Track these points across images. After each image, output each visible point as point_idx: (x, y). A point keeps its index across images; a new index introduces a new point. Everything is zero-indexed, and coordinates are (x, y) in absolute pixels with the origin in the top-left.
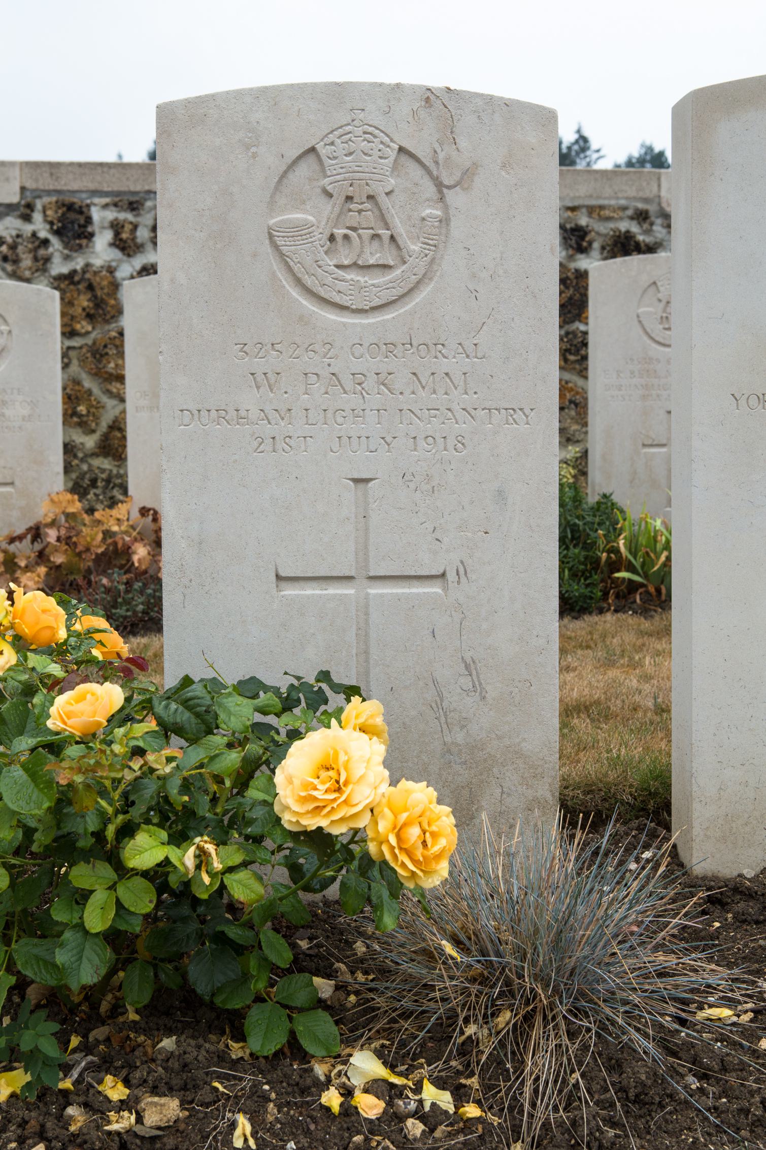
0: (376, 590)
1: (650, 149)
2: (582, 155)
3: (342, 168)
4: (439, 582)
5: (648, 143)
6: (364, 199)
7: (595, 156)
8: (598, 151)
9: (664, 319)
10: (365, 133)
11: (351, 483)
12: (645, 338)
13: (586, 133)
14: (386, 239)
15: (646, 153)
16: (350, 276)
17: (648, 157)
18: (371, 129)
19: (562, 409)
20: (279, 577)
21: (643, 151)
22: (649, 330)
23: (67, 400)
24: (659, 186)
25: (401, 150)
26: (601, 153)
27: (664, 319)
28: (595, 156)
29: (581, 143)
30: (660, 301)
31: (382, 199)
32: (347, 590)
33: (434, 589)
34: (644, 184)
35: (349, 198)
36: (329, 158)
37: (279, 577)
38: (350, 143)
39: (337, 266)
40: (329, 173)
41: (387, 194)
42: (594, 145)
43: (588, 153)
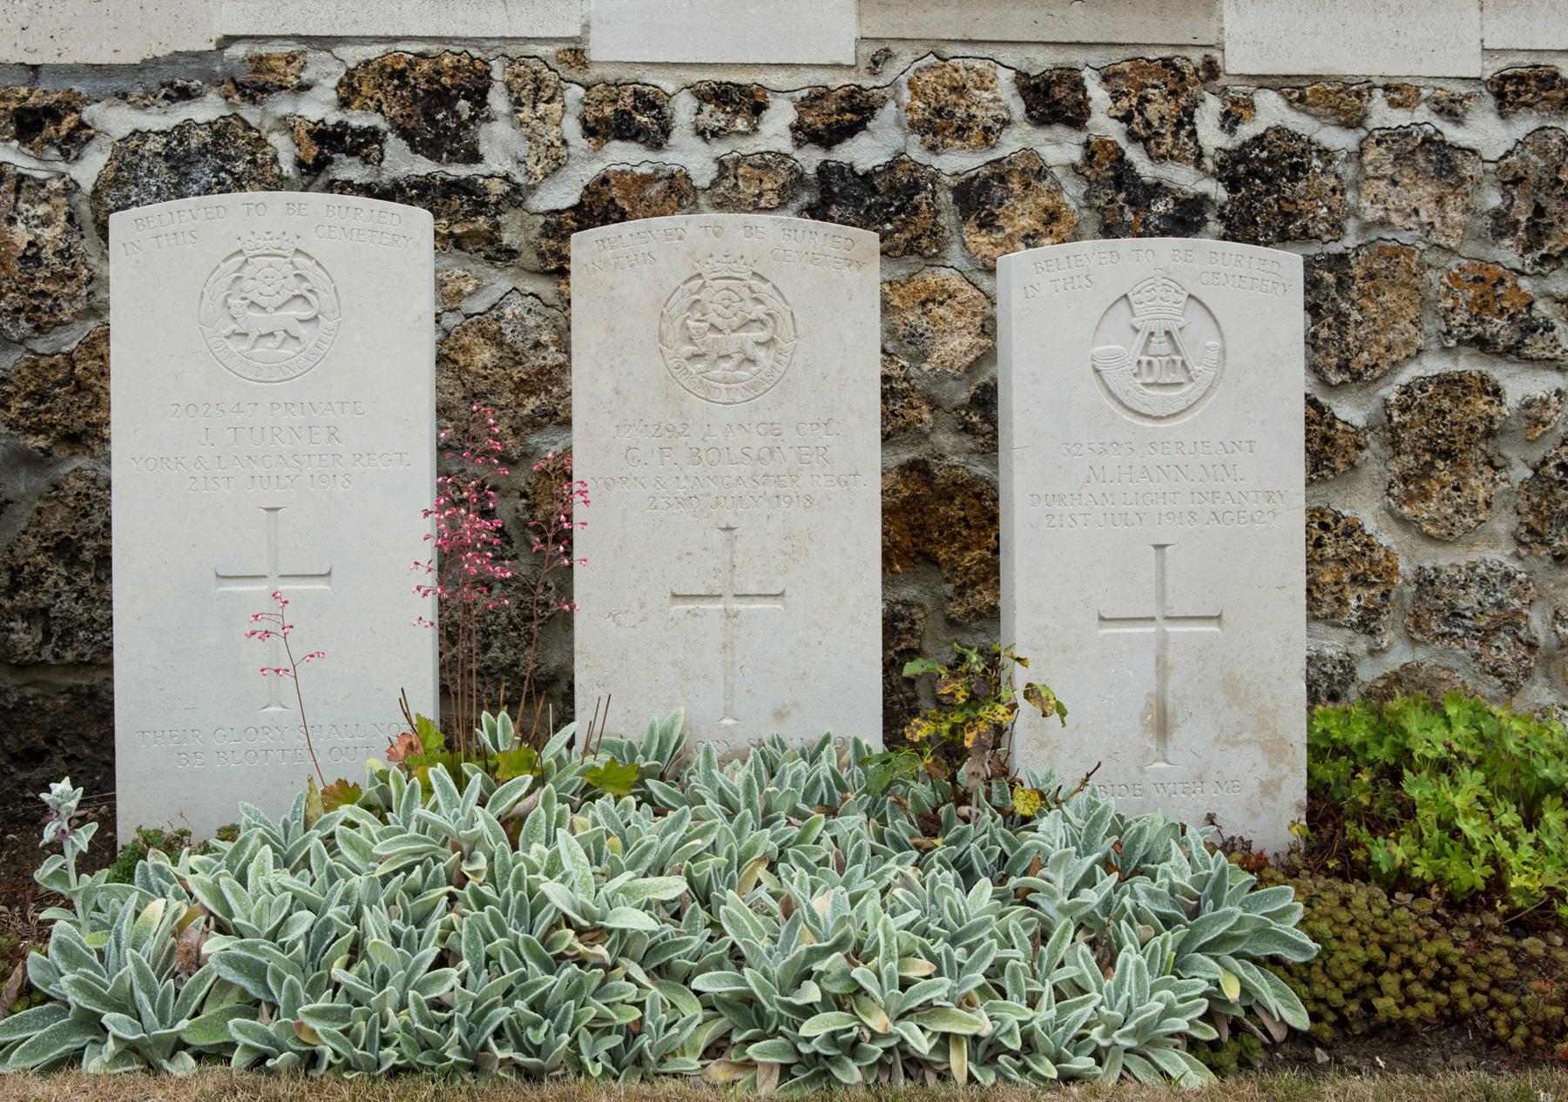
0: (1172, 629)
16: (1147, 391)
20: (1102, 619)
25: (1190, 296)
30: (1137, 331)
32: (1150, 629)
39: (1146, 385)
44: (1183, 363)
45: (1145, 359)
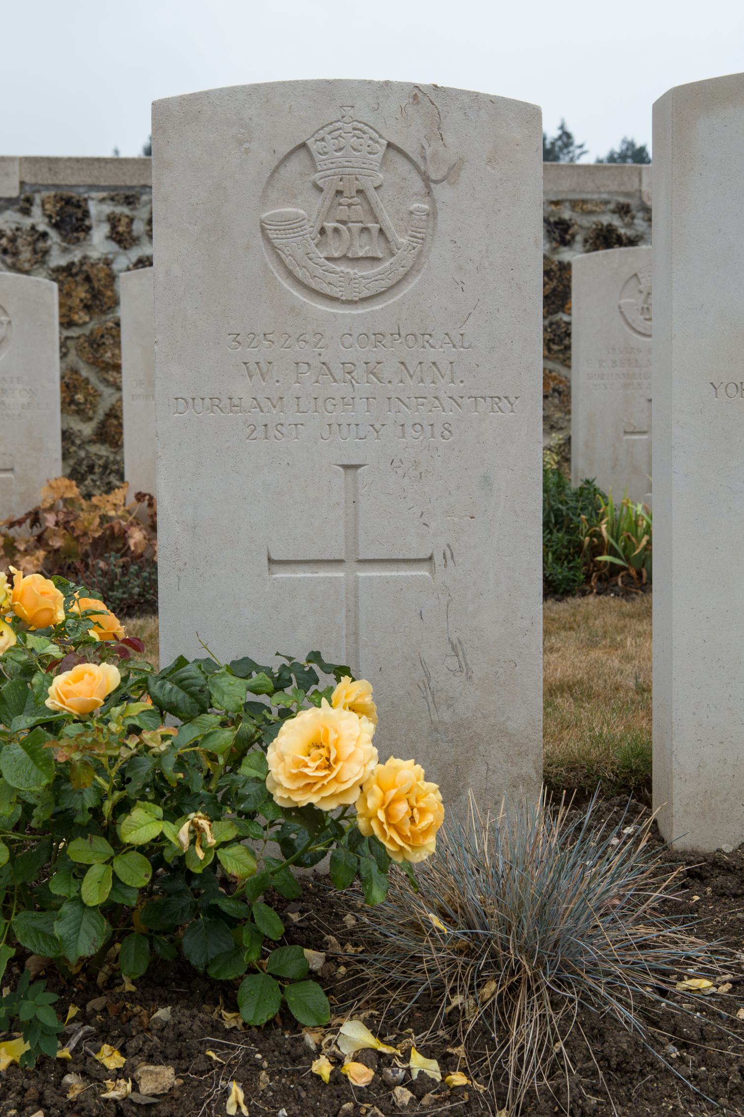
0: (365, 573)
1: (631, 145)
2: (565, 151)
3: (332, 163)
4: (426, 565)
5: (629, 139)
6: (354, 194)
7: (578, 151)
8: (581, 147)
9: (645, 310)
10: (354, 129)
11: (341, 469)
12: (627, 328)
13: (570, 129)
14: (375, 232)
15: (627, 149)
16: (341, 268)
17: (630, 153)
18: (360, 126)
19: (545, 397)
20: (271, 561)
21: (624, 147)
22: (630, 321)
23: (65, 389)
24: (640, 181)
25: (390, 145)
26: (585, 148)
27: (645, 310)
28: (578, 151)
29: (565, 139)
30: (641, 292)
31: (371, 193)
33: (422, 572)
34: (626, 179)
35: (339, 193)
36: (320, 153)
37: (271, 561)
38: (340, 139)
39: (328, 259)
40: (319, 168)
41: (376, 188)
42: (577, 141)
43: (571, 149)
44: (381, 230)
45: (645, 306)
